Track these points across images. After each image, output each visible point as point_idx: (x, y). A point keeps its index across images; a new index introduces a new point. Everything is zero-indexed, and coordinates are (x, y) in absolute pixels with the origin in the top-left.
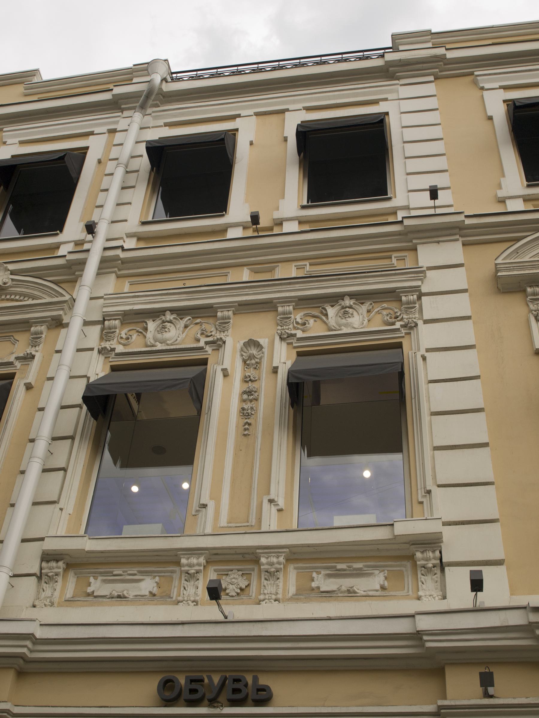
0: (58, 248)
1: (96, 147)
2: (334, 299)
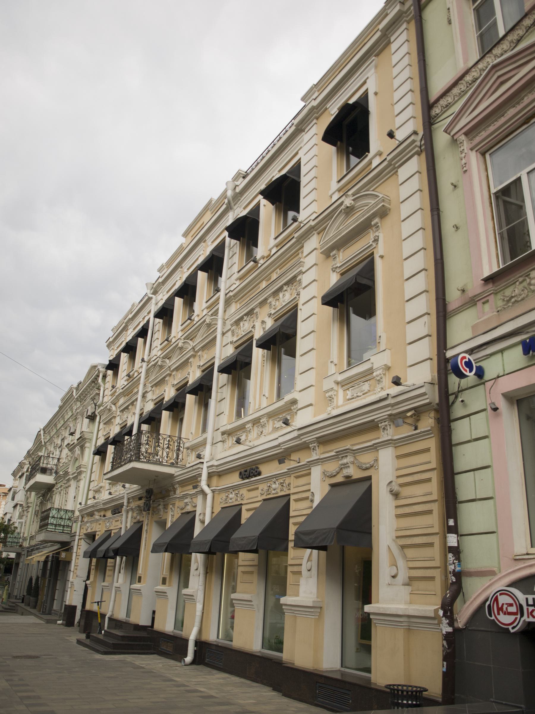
2: (280, 289)
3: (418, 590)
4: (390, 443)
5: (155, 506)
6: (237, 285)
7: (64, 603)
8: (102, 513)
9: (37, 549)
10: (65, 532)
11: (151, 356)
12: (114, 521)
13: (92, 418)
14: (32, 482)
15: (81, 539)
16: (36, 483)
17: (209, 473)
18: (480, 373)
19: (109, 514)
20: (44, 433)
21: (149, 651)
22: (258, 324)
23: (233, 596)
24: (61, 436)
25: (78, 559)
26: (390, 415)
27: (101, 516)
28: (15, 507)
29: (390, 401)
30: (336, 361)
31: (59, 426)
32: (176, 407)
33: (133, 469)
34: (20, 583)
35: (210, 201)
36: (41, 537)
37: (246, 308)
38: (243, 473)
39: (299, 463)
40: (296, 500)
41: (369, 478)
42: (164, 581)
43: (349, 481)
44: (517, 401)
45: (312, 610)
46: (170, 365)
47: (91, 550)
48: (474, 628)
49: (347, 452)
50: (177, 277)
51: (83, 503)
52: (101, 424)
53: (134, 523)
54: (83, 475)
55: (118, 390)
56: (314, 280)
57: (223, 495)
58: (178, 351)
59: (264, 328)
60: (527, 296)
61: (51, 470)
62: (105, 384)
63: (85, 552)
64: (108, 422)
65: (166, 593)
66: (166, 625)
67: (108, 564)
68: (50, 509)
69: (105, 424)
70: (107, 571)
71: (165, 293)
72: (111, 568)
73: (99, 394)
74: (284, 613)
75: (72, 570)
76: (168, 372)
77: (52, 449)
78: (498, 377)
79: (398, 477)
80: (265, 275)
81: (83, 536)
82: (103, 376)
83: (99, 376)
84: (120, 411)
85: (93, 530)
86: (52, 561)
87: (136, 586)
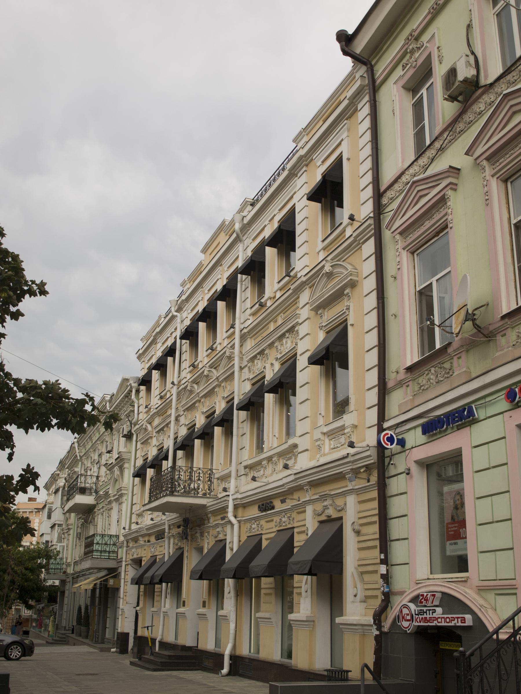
0: (297, 275)
1: (344, 149)
2: (283, 336)
3: (370, 606)
4: (352, 492)
5: (193, 533)
6: (251, 321)
7: (116, 631)
8: (146, 539)
9: (83, 575)
10: (111, 558)
11: (182, 377)
12: (158, 546)
13: (129, 436)
14: (71, 504)
15: (128, 565)
16: (76, 505)
17: (235, 505)
18: (402, 443)
19: (153, 539)
20: (79, 445)
21: (194, 668)
22: (268, 366)
23: (258, 615)
24: (97, 450)
25: (126, 585)
26: (352, 469)
27: (145, 541)
28: (53, 527)
29: (350, 459)
30: (323, 414)
31: (95, 439)
32: (206, 435)
33: (167, 503)
34: (67, 613)
35: (223, 222)
36: (86, 564)
37: (258, 348)
38: (261, 506)
39: (299, 501)
40: (299, 533)
41: (341, 518)
42: (204, 606)
43: (330, 520)
44: (427, 465)
45: (307, 623)
46: (198, 391)
47: (137, 576)
48: (394, 631)
49: (326, 497)
50: (199, 297)
51: (127, 528)
52: (139, 443)
53: (177, 549)
54: (125, 498)
55: (152, 410)
56: (307, 334)
57: (248, 525)
58: (205, 379)
59: (273, 370)
60: (430, 386)
61: (90, 489)
62: (138, 400)
63: (132, 579)
64: (146, 442)
65: (205, 615)
66: (209, 645)
67: (156, 590)
68: (94, 535)
69: (142, 443)
70: (155, 596)
71: (189, 311)
72: (158, 594)
73: (133, 411)
74: (292, 627)
75: (122, 596)
76: (197, 399)
77: (89, 465)
78: (412, 448)
79: (359, 518)
80: (271, 317)
81: (130, 562)
82: (136, 391)
83: (132, 391)
84: (156, 432)
85: (139, 556)
86: (100, 588)
87: (182, 610)
